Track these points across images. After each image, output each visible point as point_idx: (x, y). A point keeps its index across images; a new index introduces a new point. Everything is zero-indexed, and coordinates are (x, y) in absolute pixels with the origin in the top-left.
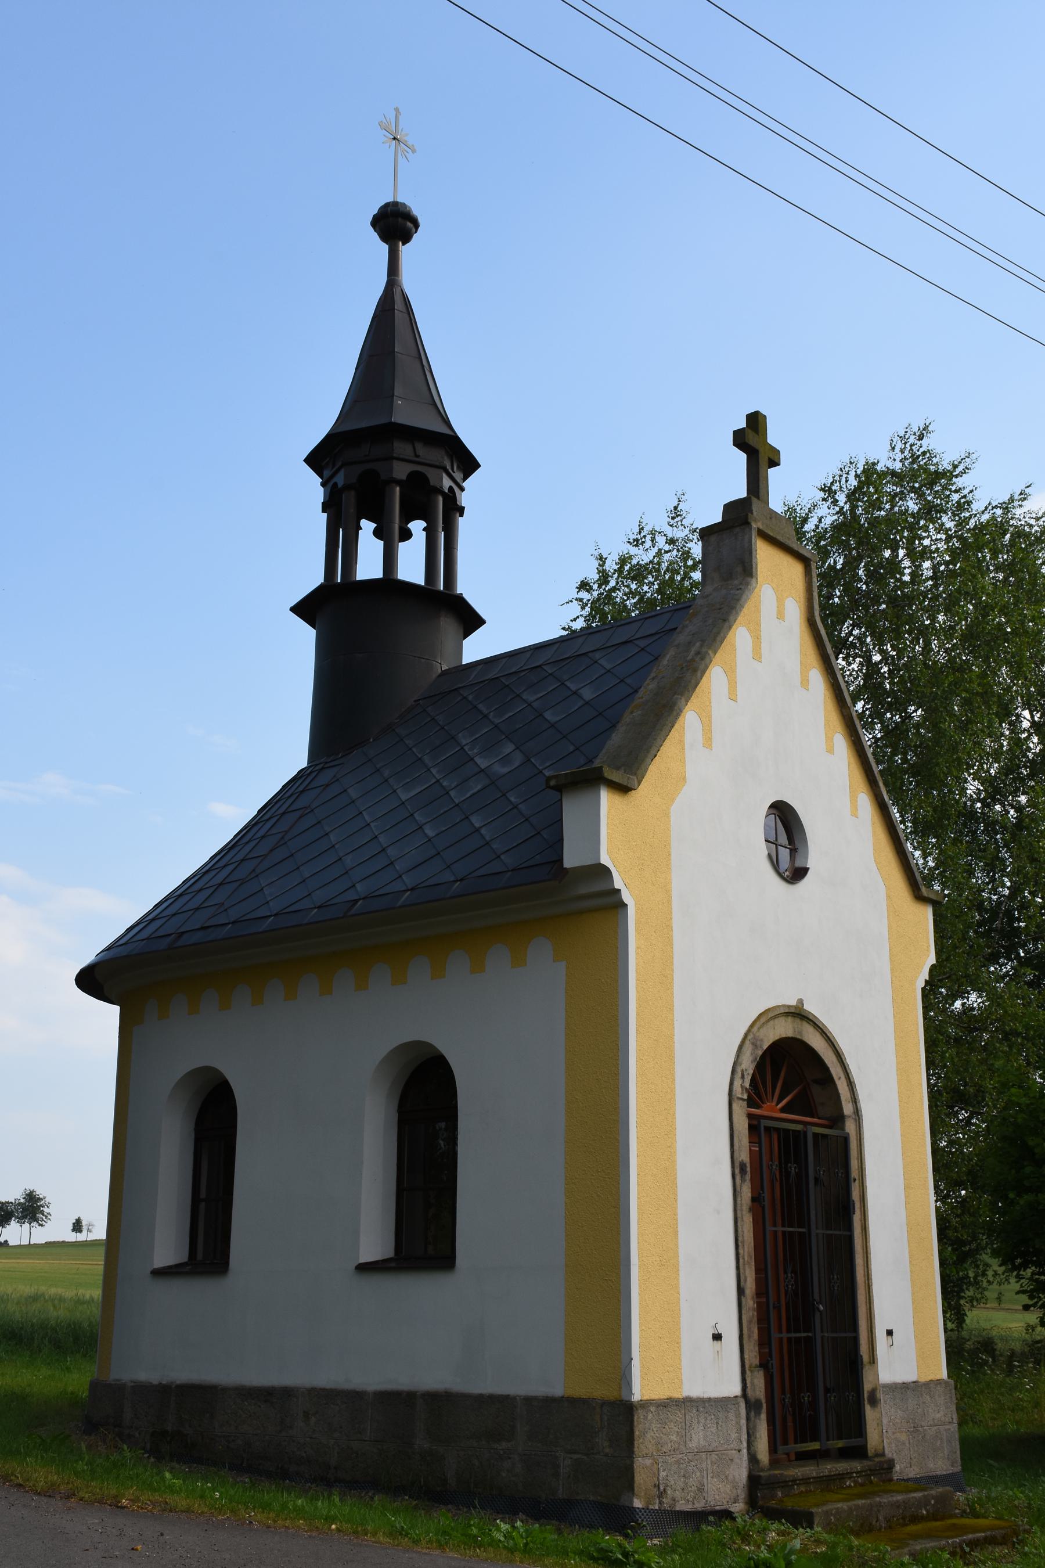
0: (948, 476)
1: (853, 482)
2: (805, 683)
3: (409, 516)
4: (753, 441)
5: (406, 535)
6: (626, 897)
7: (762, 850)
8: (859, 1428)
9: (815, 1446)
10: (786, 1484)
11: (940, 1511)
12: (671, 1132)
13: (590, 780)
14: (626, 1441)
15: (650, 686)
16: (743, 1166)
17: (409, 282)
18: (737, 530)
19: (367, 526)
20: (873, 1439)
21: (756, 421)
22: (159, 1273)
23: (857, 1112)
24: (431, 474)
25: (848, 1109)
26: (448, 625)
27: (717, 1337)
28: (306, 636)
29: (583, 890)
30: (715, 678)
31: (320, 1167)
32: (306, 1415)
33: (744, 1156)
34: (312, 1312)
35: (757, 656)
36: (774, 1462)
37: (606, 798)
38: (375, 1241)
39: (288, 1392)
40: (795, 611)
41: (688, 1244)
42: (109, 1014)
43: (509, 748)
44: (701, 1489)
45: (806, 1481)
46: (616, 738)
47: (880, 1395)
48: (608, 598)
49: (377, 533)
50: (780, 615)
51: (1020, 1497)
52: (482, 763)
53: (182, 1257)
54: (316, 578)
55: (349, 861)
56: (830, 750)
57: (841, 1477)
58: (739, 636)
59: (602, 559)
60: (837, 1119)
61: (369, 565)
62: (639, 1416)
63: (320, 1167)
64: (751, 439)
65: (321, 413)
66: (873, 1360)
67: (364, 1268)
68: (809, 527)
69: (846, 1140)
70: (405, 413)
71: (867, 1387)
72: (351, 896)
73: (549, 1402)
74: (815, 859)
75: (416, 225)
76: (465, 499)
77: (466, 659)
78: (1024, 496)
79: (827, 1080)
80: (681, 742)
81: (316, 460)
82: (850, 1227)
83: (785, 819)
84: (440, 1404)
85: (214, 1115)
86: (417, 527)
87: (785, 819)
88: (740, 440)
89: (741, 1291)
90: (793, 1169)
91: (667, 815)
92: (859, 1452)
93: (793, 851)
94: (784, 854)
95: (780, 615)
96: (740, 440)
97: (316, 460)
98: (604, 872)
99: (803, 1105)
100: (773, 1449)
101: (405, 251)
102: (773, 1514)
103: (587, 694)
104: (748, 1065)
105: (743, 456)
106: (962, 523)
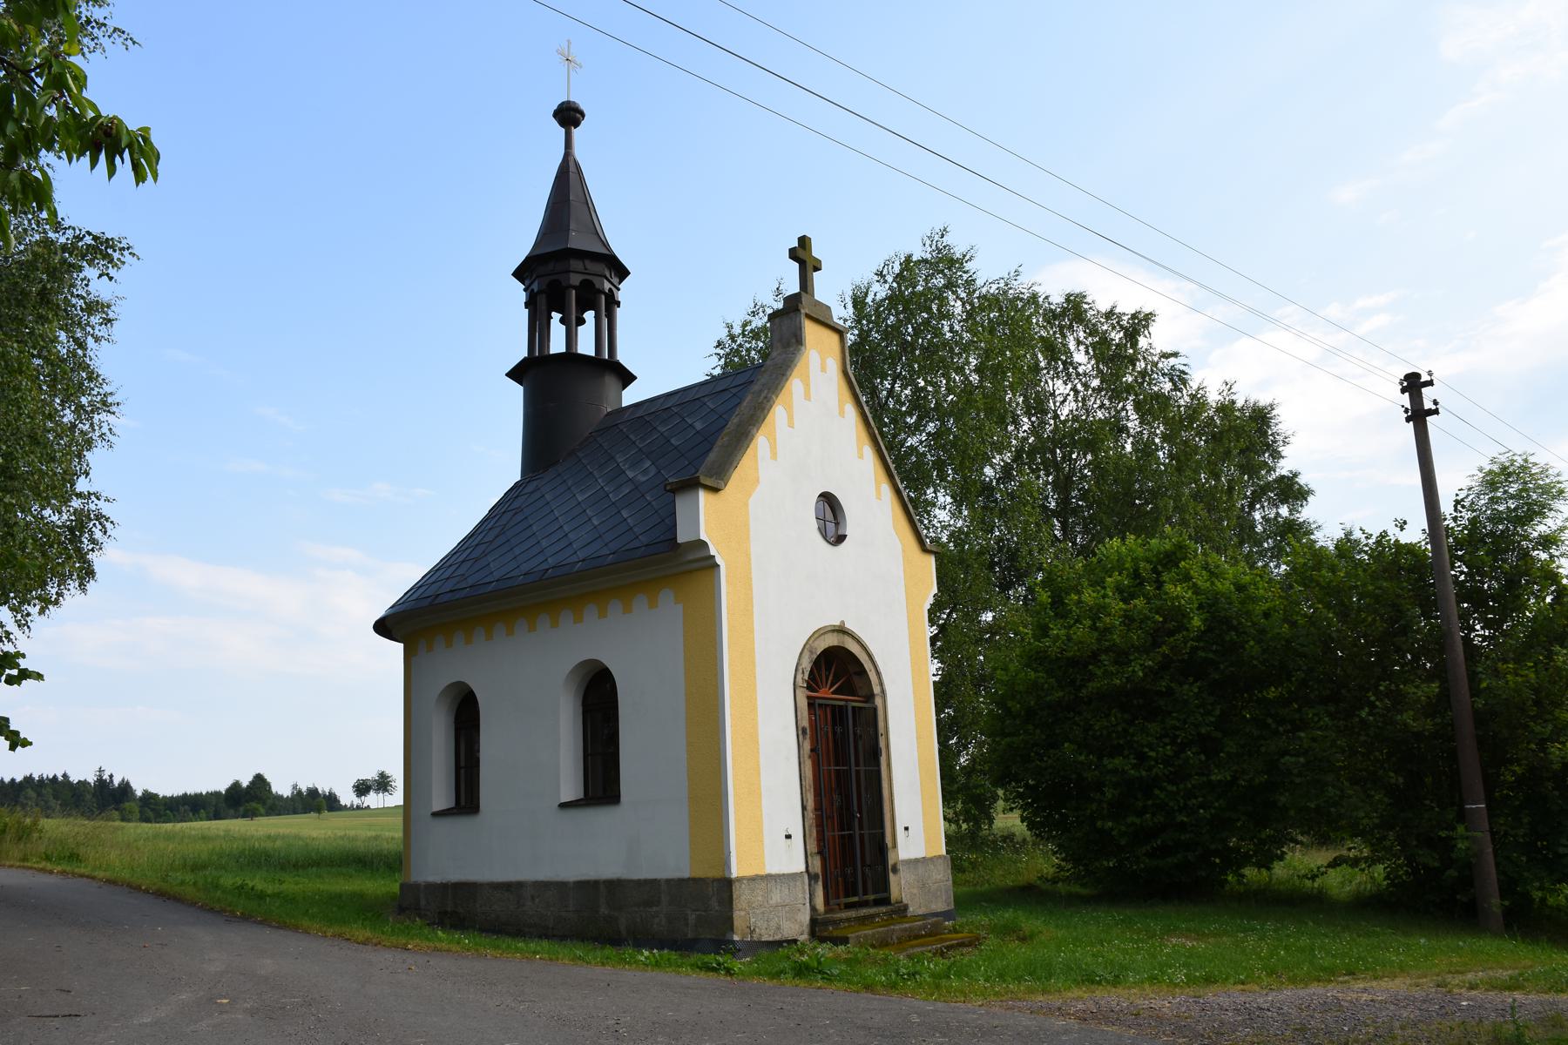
0: (960, 262)
1: (897, 269)
2: (842, 413)
3: (583, 309)
4: (802, 255)
5: (581, 322)
6: (719, 560)
7: (814, 524)
8: (885, 886)
9: (855, 899)
10: (835, 923)
11: (934, 932)
12: (754, 709)
13: (691, 485)
14: (728, 902)
15: (735, 420)
16: (804, 730)
17: (579, 153)
18: (790, 319)
19: (556, 316)
20: (895, 893)
21: (804, 241)
22: (435, 814)
23: (883, 691)
24: (596, 280)
25: (876, 690)
26: (611, 381)
27: (788, 837)
28: (517, 391)
29: (691, 557)
30: (778, 413)
31: (534, 744)
32: (533, 898)
33: (805, 723)
34: (534, 833)
35: (807, 397)
36: (826, 912)
37: (703, 496)
38: (570, 788)
39: (520, 885)
40: (833, 366)
41: (766, 781)
42: (397, 649)
43: (648, 463)
44: (778, 928)
45: (848, 920)
46: (712, 456)
47: (900, 867)
48: (737, 352)
49: (562, 321)
50: (823, 369)
51: (984, 920)
52: (630, 474)
53: (452, 804)
54: (523, 353)
55: (544, 543)
56: (861, 457)
57: (872, 916)
58: (794, 384)
59: (730, 327)
60: (870, 697)
61: (557, 345)
62: (736, 886)
63: (534, 744)
64: (801, 254)
65: (523, 244)
66: (895, 846)
67: (564, 806)
68: (869, 300)
69: (875, 709)
70: (577, 241)
71: (891, 862)
72: (544, 566)
73: (681, 881)
74: (850, 529)
75: (583, 115)
76: (620, 296)
77: (624, 404)
78: (1017, 273)
79: (862, 672)
80: (755, 456)
81: (519, 274)
82: (878, 765)
83: (829, 503)
84: (614, 886)
85: (465, 712)
86: (589, 316)
87: (829, 503)
88: (793, 254)
89: (804, 808)
90: (839, 730)
91: (746, 505)
92: (886, 901)
93: (837, 524)
94: (831, 526)
95: (823, 369)
96: (793, 254)
97: (519, 274)
98: (704, 545)
99: (847, 689)
100: (827, 902)
101: (577, 133)
102: (822, 940)
103: (699, 426)
104: (807, 665)
105: (797, 265)
106: (970, 294)
